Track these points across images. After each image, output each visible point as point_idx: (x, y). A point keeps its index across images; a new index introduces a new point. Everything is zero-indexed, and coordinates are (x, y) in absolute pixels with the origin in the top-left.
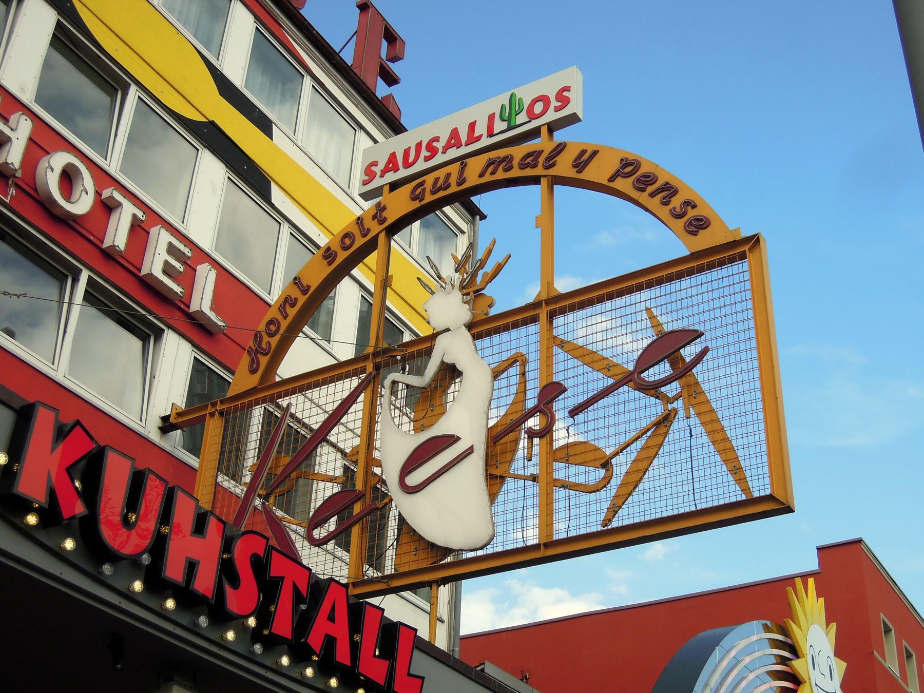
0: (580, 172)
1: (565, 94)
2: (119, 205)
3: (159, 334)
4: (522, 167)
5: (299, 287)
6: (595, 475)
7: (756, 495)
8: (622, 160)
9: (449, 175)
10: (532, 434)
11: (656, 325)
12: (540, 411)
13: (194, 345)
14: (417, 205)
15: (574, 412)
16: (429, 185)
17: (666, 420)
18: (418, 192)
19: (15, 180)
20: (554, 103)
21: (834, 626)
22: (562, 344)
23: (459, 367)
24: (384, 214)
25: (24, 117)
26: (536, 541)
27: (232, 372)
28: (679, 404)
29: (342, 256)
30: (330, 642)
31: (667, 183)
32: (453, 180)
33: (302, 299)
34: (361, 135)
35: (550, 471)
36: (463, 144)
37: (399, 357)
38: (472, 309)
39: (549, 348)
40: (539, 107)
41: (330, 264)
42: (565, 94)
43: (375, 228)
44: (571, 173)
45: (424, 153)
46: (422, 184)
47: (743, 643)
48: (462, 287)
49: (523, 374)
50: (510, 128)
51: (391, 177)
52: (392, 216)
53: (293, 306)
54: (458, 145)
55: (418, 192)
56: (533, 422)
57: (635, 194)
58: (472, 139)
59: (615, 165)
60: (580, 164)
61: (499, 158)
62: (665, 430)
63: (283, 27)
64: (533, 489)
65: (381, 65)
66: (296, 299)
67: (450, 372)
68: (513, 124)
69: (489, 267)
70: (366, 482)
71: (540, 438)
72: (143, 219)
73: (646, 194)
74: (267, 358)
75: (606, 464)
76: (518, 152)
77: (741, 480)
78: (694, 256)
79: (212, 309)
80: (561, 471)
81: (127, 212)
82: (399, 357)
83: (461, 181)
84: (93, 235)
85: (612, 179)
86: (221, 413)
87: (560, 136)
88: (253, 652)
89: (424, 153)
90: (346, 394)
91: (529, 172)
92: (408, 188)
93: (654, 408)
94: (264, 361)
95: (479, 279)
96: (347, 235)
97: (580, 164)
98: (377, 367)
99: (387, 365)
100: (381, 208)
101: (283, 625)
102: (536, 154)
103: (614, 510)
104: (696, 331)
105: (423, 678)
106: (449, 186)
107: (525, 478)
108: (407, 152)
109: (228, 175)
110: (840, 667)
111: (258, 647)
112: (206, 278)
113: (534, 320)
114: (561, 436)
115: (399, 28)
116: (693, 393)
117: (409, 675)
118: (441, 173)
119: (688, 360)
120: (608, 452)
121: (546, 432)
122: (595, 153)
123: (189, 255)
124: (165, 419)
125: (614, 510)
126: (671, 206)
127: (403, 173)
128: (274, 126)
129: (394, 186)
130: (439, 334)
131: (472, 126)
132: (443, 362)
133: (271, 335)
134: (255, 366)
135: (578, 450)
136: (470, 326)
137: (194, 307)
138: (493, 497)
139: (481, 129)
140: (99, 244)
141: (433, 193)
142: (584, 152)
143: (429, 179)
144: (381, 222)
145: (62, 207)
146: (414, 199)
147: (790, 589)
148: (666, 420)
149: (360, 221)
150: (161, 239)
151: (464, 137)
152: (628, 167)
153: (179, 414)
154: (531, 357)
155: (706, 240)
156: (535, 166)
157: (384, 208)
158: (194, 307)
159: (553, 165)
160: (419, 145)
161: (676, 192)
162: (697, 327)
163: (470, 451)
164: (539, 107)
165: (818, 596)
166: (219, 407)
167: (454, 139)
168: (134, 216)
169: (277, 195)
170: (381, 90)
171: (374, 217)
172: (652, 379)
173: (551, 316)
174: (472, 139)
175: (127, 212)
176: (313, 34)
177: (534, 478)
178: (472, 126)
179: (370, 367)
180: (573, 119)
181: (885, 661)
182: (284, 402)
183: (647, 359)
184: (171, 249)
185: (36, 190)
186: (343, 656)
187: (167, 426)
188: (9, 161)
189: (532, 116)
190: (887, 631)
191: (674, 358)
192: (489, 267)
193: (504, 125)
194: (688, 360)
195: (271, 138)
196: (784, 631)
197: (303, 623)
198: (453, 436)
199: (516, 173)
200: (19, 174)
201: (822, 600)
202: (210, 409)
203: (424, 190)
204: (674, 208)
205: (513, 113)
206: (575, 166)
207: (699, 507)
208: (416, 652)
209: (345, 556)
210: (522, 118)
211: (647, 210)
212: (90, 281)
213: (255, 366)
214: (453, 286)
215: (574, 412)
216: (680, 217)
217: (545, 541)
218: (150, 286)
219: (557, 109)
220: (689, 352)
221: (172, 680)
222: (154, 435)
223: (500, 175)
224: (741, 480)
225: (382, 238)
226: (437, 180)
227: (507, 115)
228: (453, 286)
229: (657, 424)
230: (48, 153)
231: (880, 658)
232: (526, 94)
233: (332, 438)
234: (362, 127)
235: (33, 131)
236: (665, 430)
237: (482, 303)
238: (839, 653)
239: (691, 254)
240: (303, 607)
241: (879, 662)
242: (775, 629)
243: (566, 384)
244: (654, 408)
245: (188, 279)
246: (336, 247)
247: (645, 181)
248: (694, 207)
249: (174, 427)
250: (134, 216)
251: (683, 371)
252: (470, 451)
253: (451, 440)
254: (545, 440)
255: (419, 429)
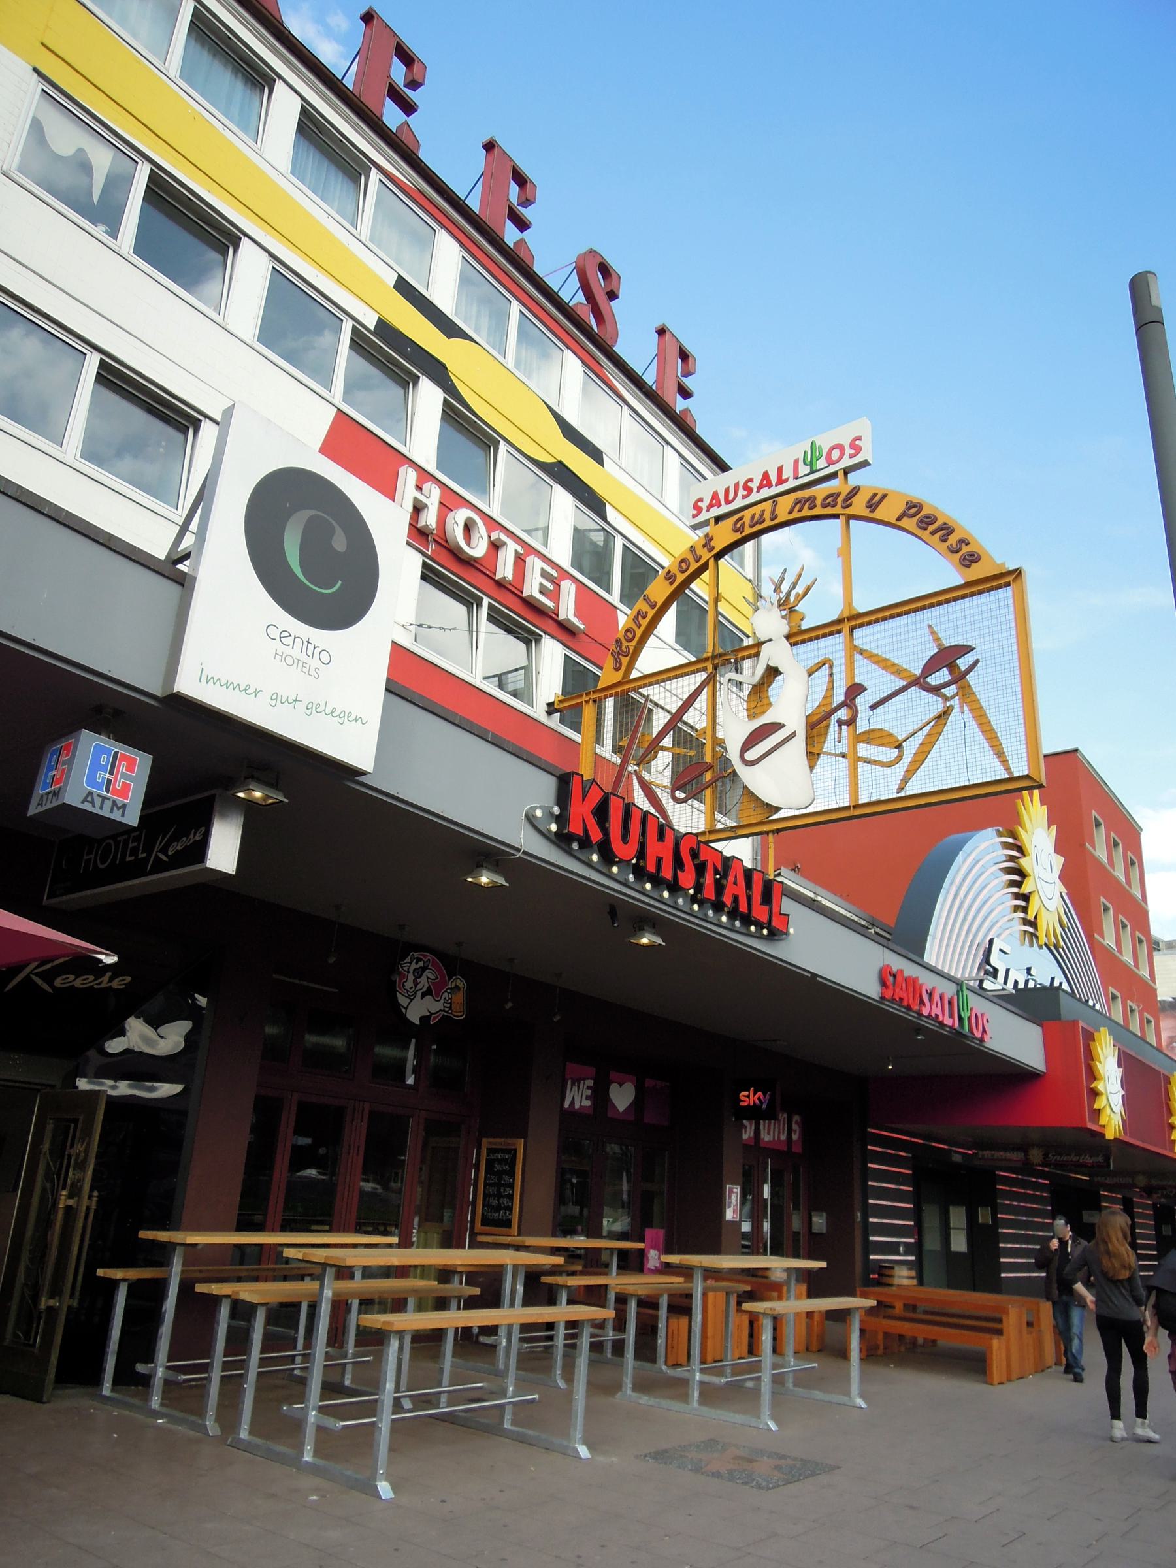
0: (872, 511)
1: (857, 442)
2: (504, 544)
3: (538, 639)
4: (824, 506)
5: (648, 603)
6: (890, 754)
7: (1016, 775)
8: (907, 503)
9: (763, 511)
10: (840, 723)
11: (937, 639)
12: (847, 705)
13: (564, 645)
14: (738, 536)
15: (873, 707)
16: (747, 520)
17: (944, 715)
18: (738, 525)
19: (433, 536)
20: (848, 451)
21: (1054, 828)
22: (861, 652)
23: (781, 669)
24: (712, 543)
25: (434, 485)
26: (846, 804)
27: (601, 669)
28: (955, 702)
29: (680, 578)
30: (736, 899)
31: (945, 524)
32: (767, 516)
33: (651, 613)
34: (668, 449)
35: (855, 752)
36: (774, 484)
37: (732, 660)
38: (789, 623)
39: (852, 656)
40: (835, 455)
41: (671, 584)
42: (857, 442)
43: (706, 555)
44: (865, 512)
45: (742, 492)
46: (741, 518)
47: (983, 846)
48: (779, 605)
49: (831, 675)
50: (812, 472)
51: (716, 512)
52: (719, 545)
53: (644, 618)
54: (769, 485)
55: (738, 525)
56: (843, 714)
57: (919, 532)
58: (781, 481)
59: (902, 508)
60: (873, 505)
61: (804, 498)
62: (944, 722)
63: (603, 367)
64: (844, 763)
65: (679, 383)
66: (647, 613)
67: (773, 672)
68: (814, 469)
69: (800, 589)
70: (713, 756)
71: (848, 726)
72: (522, 552)
73: (927, 532)
74: (628, 658)
75: (899, 747)
76: (820, 491)
77: (1004, 762)
78: (967, 585)
79: (575, 616)
80: (863, 750)
81: (511, 549)
82: (732, 660)
83: (774, 518)
84: (489, 570)
85: (899, 519)
86: (594, 701)
87: (854, 479)
88: (692, 909)
89: (742, 492)
90: (693, 688)
91: (829, 511)
92: (730, 522)
93: (935, 705)
94: (625, 661)
95: (792, 598)
96: (683, 561)
97: (873, 505)
98: (716, 667)
99: (723, 664)
100: (709, 539)
101: (709, 893)
102: (834, 496)
103: (905, 781)
104: (970, 646)
105: (788, 915)
106: (764, 521)
107: (835, 755)
108: (727, 491)
109: (575, 503)
110: (1059, 861)
111: (696, 907)
112: (568, 591)
113: (839, 632)
114: (862, 726)
115: (690, 348)
116: (966, 693)
117: (781, 914)
118: (757, 510)
119: (963, 669)
120: (900, 738)
121: (851, 722)
122: (884, 496)
123: (556, 575)
124: (550, 705)
125: (905, 781)
126: (948, 543)
127: (725, 509)
128: (604, 455)
129: (718, 519)
130: (763, 643)
131: (780, 470)
132: (768, 665)
133: (630, 641)
134: (618, 665)
135: (877, 735)
136: (788, 637)
137: (561, 617)
138: (812, 768)
139: (788, 473)
140: (493, 577)
141: (752, 526)
142: (875, 495)
143: (747, 514)
144: (710, 550)
145: (467, 553)
146: (736, 531)
147: (1019, 802)
148: (944, 715)
149: (692, 549)
150: (535, 566)
151: (774, 480)
152: (913, 508)
153: (560, 701)
154: (836, 663)
155: (978, 571)
156: (834, 506)
157: (712, 539)
158: (561, 617)
159: (850, 505)
160: (737, 485)
161: (952, 531)
162: (969, 643)
163: (794, 735)
164: (835, 455)
165: (1042, 804)
166: (592, 696)
167: (766, 481)
168: (516, 551)
169: (611, 514)
170: (680, 404)
171: (704, 546)
172: (933, 683)
173: (852, 629)
174: (781, 481)
175: (511, 549)
176: (627, 369)
177: (843, 755)
178: (780, 470)
179: (710, 669)
180: (865, 464)
181: (1095, 850)
182: (644, 691)
183: (931, 666)
184: (544, 574)
185: (447, 542)
186: (743, 908)
187: (551, 709)
188: (428, 524)
189: (831, 462)
190: (1098, 825)
191: (952, 667)
192: (800, 589)
193: (807, 469)
194: (963, 669)
195: (603, 466)
196: (1013, 835)
197: (719, 888)
198: (780, 724)
199: (818, 511)
200: (435, 532)
201: (1045, 807)
202: (585, 698)
203: (744, 523)
204: (951, 545)
205: (814, 459)
206: (868, 507)
207: (971, 783)
208: (783, 897)
209: (702, 807)
210: (821, 463)
211: (927, 544)
212: (490, 606)
213: (618, 665)
214: (772, 604)
215: (873, 707)
216: (957, 552)
217: (854, 804)
218: (531, 605)
219: (851, 456)
220: (963, 663)
221: (643, 930)
222: (542, 717)
223: (806, 512)
224: (1004, 762)
225: (712, 562)
226: (754, 515)
227: (809, 460)
228: (772, 604)
229: (939, 717)
230: (452, 510)
231: (1091, 848)
232: (825, 442)
233: (685, 718)
234: (668, 443)
235: (442, 496)
236: (944, 722)
237: (794, 616)
238: (1058, 850)
239: (965, 583)
240: (718, 877)
241: (1089, 851)
242: (1005, 833)
243: (866, 684)
244: (935, 705)
245: (555, 595)
246: (675, 570)
247: (927, 521)
248: (967, 544)
249: (557, 711)
250: (516, 551)
251: (959, 678)
252: (794, 735)
253: (776, 727)
254: (851, 727)
255: (752, 716)
